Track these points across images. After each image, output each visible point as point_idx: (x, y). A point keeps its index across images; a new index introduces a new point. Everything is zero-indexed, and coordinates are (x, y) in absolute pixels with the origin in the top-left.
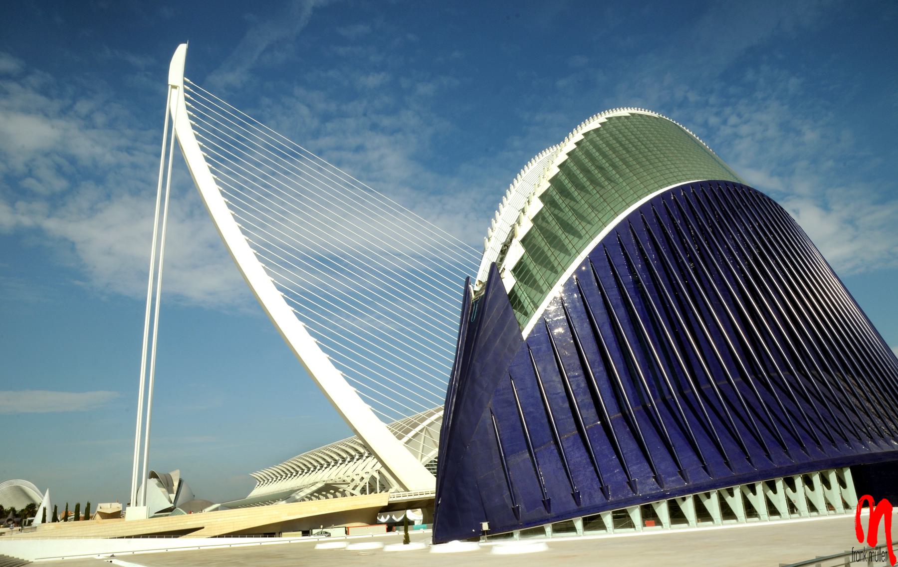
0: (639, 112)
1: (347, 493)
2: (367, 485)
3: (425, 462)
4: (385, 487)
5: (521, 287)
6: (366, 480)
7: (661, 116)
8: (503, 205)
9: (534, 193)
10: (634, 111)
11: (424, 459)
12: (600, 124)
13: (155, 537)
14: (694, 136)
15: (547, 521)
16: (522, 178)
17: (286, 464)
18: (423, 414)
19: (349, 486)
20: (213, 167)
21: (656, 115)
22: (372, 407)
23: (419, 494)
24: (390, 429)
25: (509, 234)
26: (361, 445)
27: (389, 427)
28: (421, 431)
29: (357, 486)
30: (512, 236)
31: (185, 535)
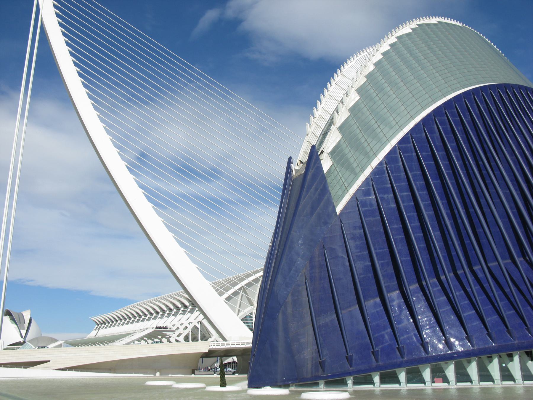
0: (446, 21)
1: (172, 339)
2: (190, 333)
3: (241, 316)
4: (205, 338)
5: (337, 169)
6: (189, 329)
7: (464, 25)
8: (324, 96)
9: (352, 86)
10: (442, 20)
11: (240, 314)
12: (412, 29)
13: (8, 367)
14: (492, 44)
15: (349, 374)
16: (342, 73)
17: (121, 311)
18: (242, 275)
19: (174, 333)
20: (80, 71)
21: (460, 25)
22: (199, 266)
23: (235, 344)
24: (212, 286)
25: (323, 129)
26: (187, 299)
27: (212, 284)
28: (240, 289)
29: (182, 334)
30: (331, 123)
31: (33, 366)
